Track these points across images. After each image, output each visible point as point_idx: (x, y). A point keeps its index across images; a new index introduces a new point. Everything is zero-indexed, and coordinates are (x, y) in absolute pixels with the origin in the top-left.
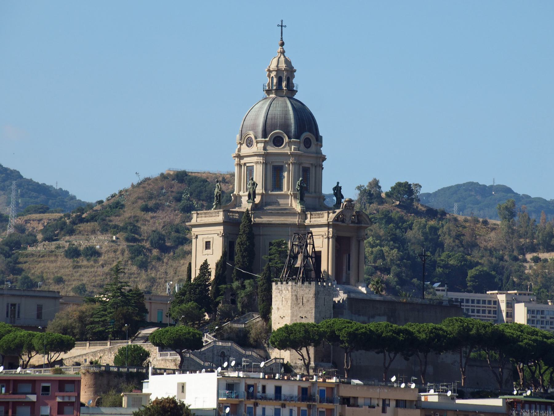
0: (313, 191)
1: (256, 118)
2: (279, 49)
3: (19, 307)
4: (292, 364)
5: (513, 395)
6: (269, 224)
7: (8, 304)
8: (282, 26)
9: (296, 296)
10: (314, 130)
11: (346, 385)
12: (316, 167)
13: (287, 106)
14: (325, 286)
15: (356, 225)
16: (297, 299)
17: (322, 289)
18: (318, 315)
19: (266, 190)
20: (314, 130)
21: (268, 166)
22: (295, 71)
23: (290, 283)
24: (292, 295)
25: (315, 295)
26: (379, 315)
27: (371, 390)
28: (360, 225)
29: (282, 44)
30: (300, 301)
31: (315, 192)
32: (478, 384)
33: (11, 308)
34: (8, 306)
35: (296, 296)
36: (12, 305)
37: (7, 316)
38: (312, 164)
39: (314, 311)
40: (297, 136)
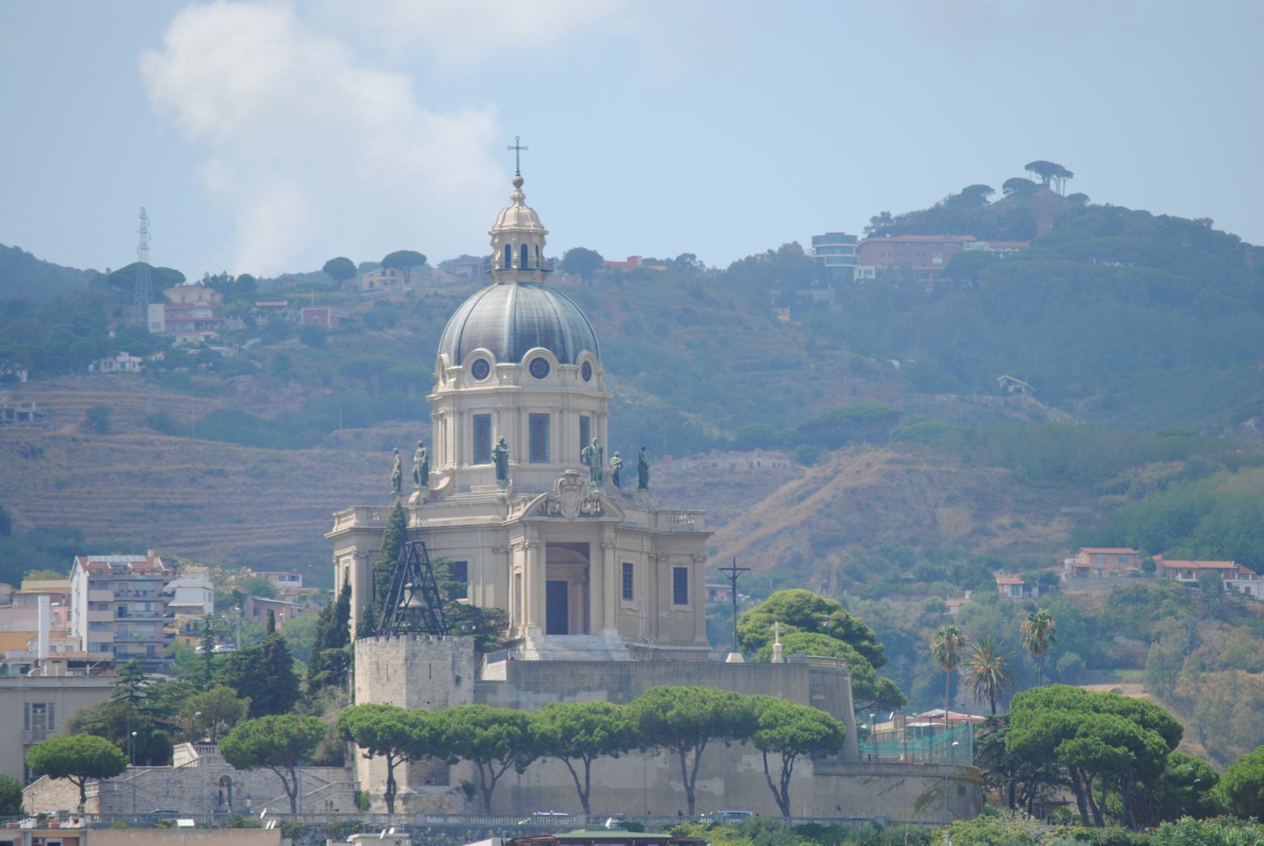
0: (557, 457)
1: (453, 331)
2: (513, 191)
3: (51, 708)
4: (372, 792)
5: (605, 829)
6: (445, 528)
7: (26, 705)
8: (518, 148)
9: (377, 663)
10: (558, 343)
11: (104, 831)
12: (561, 412)
13: (504, 302)
14: (430, 643)
15: (592, 520)
16: (378, 670)
17: (424, 648)
18: (415, 698)
19: (461, 463)
20: (558, 343)
21: (465, 417)
22: (546, 233)
23: (403, 637)
24: (371, 663)
25: (406, 659)
26: (589, 689)
27: (165, 838)
28: (602, 519)
29: (519, 183)
30: (383, 672)
31: (561, 460)
32: (839, 808)
33: (35, 711)
34: (27, 709)
35: (377, 663)
36: (36, 706)
37: (27, 727)
38: (593, 412)
39: (404, 691)
40: (515, 358)
